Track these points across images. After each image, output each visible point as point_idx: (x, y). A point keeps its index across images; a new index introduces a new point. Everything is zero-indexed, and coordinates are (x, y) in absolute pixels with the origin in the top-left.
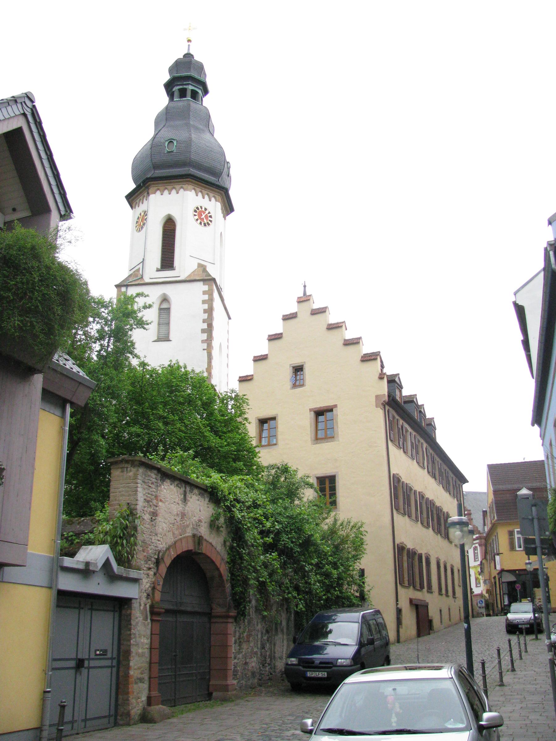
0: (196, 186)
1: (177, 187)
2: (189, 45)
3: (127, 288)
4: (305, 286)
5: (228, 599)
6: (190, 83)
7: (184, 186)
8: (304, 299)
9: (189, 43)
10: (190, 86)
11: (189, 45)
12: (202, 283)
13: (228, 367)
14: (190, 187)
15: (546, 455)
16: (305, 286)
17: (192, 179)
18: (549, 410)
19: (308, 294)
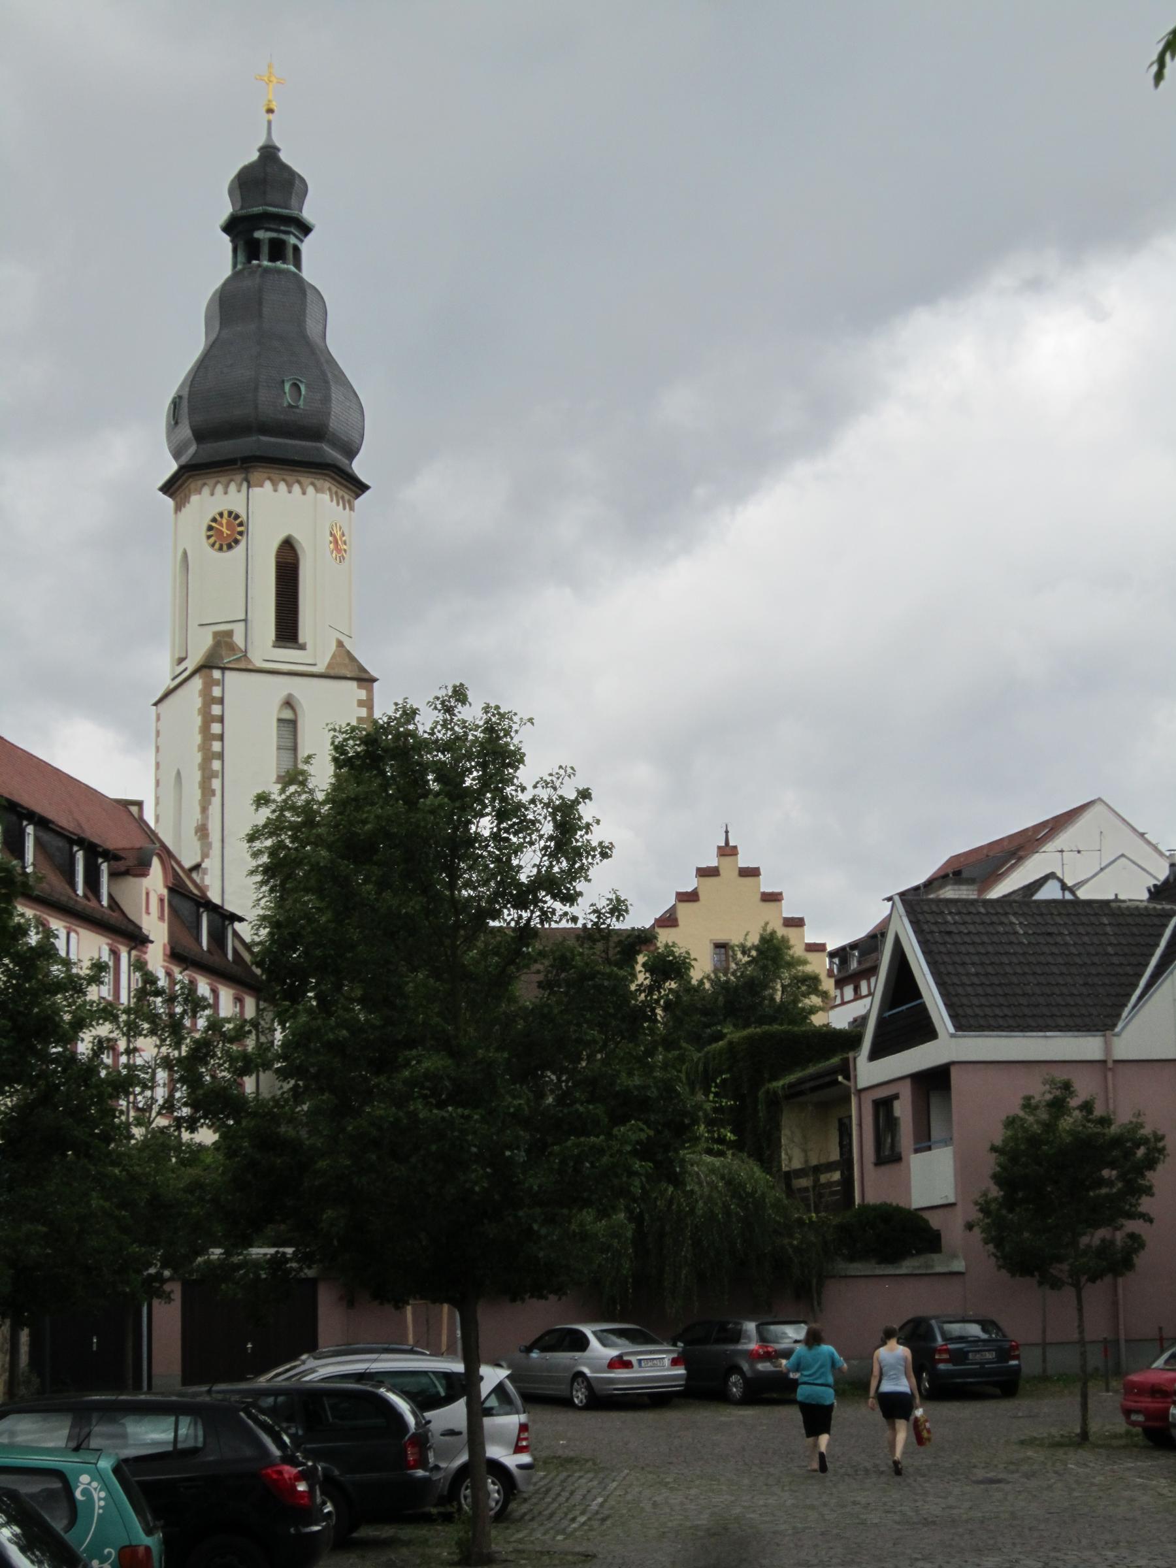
0: (335, 483)
1: (305, 480)
2: (269, 123)
3: (223, 674)
4: (727, 832)
5: (615, 1244)
6: (292, 230)
7: (316, 481)
8: (728, 851)
9: (271, 116)
10: (292, 236)
11: (269, 123)
12: (354, 684)
13: (179, 773)
14: (327, 485)
15: (121, 854)
16: (727, 832)
17: (333, 472)
18: (976, 1037)
19: (731, 844)
